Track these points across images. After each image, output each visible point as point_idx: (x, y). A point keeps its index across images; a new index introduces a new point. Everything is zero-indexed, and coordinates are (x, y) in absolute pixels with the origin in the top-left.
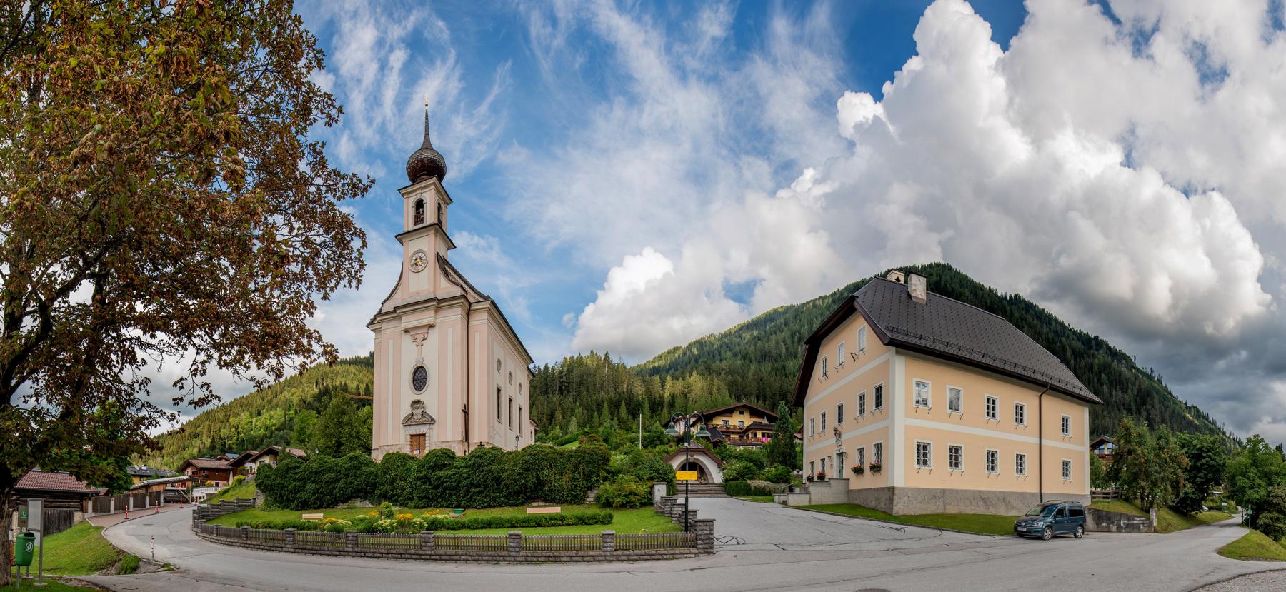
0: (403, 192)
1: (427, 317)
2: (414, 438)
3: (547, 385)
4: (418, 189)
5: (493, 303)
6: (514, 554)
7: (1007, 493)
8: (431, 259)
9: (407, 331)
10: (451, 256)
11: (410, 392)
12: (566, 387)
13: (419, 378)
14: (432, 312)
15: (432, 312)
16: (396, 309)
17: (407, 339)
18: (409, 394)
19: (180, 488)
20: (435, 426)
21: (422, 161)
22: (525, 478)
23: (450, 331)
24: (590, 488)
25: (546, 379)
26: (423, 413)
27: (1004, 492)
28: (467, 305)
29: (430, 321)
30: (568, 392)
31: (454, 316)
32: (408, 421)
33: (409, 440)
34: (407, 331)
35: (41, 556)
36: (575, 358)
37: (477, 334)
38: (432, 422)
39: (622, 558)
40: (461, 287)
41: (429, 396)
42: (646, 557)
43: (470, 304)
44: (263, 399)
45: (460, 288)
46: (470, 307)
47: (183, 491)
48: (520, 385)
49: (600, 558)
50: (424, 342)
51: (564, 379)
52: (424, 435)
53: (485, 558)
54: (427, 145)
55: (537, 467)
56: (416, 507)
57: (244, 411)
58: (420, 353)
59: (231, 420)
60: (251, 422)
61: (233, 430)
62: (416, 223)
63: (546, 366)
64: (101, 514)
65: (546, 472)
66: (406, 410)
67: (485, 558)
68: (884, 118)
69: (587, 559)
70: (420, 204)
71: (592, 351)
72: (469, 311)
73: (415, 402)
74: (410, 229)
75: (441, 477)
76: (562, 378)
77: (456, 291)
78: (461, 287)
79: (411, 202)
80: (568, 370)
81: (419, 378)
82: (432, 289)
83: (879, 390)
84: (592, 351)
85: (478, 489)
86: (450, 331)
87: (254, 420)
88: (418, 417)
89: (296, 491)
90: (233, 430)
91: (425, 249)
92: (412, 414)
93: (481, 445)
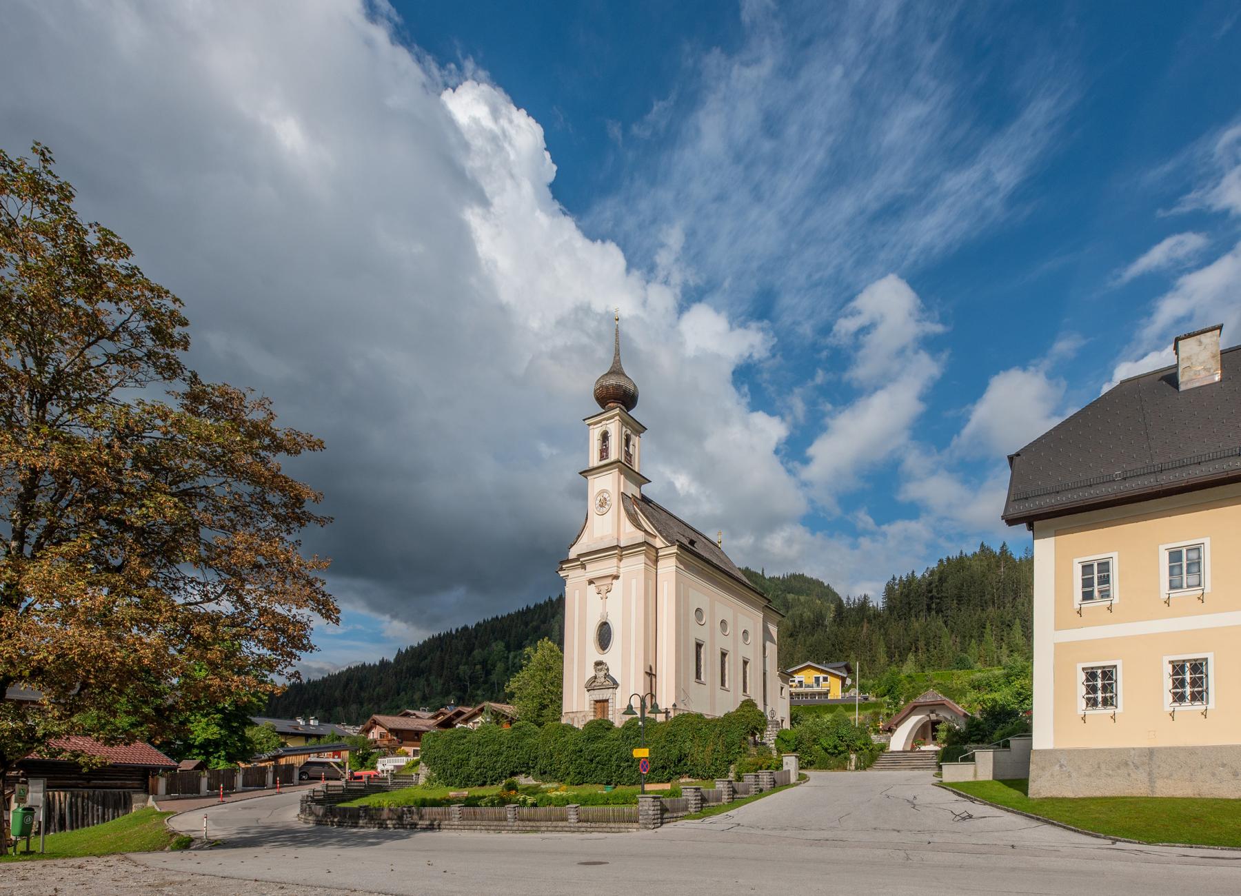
1: (607, 566)
2: (598, 704)
4: (604, 420)
6: (510, 824)
8: (614, 499)
9: (591, 582)
10: (647, 490)
13: (604, 636)
14: (615, 560)
15: (615, 560)
16: (580, 556)
18: (594, 654)
19: (331, 760)
21: (607, 387)
23: (634, 581)
26: (607, 676)
29: (613, 571)
31: (635, 565)
32: (591, 686)
33: (592, 706)
34: (591, 582)
37: (666, 583)
38: (615, 685)
39: (583, 829)
41: (612, 658)
42: (599, 829)
43: (657, 550)
44: (527, 624)
46: (657, 553)
47: (336, 763)
49: (566, 829)
52: (607, 701)
53: (492, 828)
54: (616, 371)
56: (572, 784)
57: (496, 640)
58: (604, 606)
59: (476, 652)
60: (508, 658)
61: (478, 667)
62: (602, 458)
64: (189, 795)
65: (688, 744)
66: (590, 672)
67: (492, 828)
68: (1047, 364)
69: (558, 829)
70: (605, 437)
72: (657, 557)
73: (598, 664)
75: (594, 750)
76: (930, 591)
79: (595, 434)
80: (940, 579)
81: (604, 636)
86: (634, 581)
87: (512, 655)
88: (603, 680)
89: (461, 764)
90: (478, 667)
91: (609, 488)
92: (595, 677)
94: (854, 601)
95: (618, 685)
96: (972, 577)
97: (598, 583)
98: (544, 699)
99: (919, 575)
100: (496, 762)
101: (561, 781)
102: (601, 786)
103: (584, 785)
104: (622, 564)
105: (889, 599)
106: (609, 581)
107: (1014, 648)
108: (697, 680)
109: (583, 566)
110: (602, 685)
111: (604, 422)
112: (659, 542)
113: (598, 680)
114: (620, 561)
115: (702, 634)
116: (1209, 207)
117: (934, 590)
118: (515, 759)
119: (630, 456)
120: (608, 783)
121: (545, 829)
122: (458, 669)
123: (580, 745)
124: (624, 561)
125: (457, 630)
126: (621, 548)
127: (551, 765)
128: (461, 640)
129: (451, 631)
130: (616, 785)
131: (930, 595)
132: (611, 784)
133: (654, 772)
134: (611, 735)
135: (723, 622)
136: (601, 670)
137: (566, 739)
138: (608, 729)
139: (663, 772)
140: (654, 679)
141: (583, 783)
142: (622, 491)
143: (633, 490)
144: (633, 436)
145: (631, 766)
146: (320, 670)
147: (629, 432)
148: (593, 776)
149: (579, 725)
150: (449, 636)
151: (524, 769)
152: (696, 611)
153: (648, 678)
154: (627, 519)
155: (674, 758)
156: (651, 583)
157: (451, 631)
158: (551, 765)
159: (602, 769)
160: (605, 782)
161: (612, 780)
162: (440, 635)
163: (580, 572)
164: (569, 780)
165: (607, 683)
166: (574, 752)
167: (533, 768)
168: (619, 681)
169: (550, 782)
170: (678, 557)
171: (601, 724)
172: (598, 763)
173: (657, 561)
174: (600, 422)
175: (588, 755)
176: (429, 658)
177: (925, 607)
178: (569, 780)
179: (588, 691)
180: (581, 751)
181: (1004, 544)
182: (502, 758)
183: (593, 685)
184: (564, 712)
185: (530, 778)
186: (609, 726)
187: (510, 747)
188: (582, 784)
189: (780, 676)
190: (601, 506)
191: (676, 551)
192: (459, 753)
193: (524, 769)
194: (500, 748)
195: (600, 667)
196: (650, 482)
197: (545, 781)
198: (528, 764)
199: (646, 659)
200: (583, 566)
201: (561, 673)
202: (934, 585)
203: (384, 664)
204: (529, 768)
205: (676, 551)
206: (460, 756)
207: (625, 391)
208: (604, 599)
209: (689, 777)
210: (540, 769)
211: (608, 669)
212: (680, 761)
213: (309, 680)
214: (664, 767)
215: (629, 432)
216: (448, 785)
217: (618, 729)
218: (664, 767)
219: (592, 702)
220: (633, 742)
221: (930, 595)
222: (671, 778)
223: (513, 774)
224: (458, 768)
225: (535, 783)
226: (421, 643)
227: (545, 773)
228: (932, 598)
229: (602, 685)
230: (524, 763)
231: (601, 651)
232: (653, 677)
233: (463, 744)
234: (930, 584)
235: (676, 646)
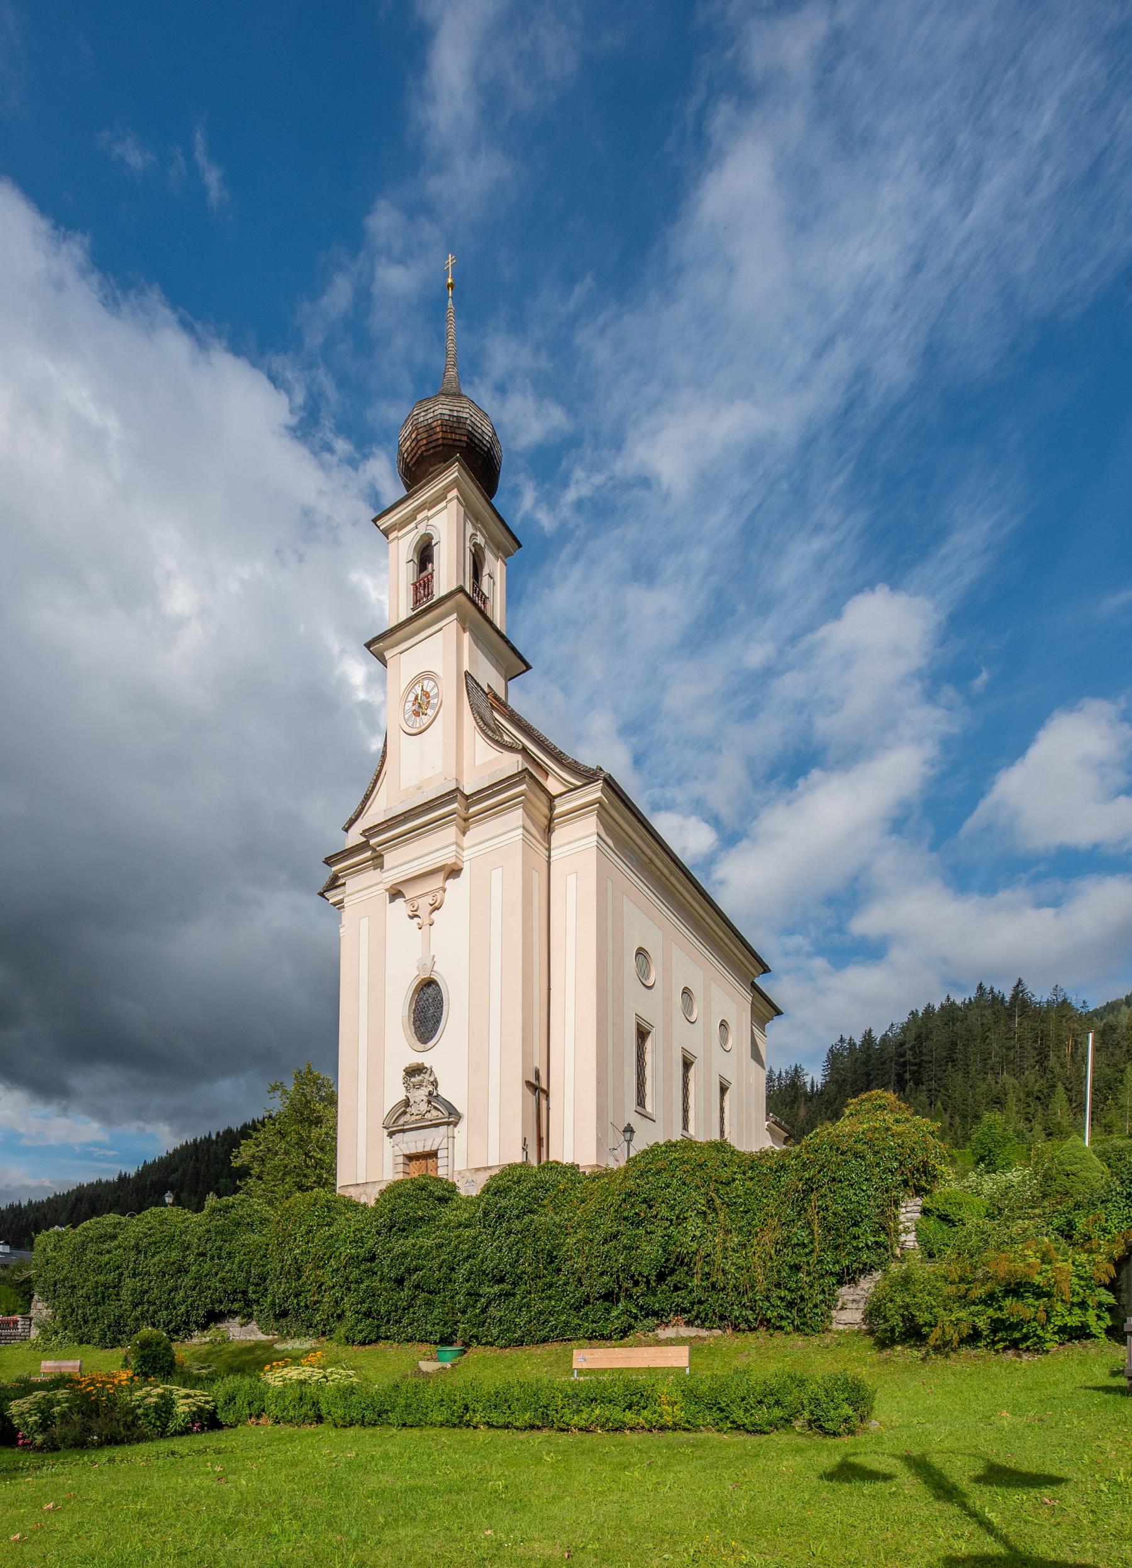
0: (385, 523)
2: (414, 1165)
3: (868, 1074)
5: (610, 784)
12: (913, 1073)
15: (450, 833)
20: (461, 1130)
21: (429, 428)
22: (629, 1248)
23: (497, 875)
24: (847, 1277)
25: (865, 1063)
26: (433, 1098)
29: (446, 857)
30: (918, 1082)
33: (401, 1168)
34: (396, 894)
36: (937, 1007)
38: (453, 1117)
40: (524, 751)
43: (551, 798)
45: (518, 757)
46: (552, 809)
48: (723, 1024)
51: (909, 1056)
55: (664, 1211)
56: (349, 1340)
58: (427, 943)
63: (869, 1034)
65: (694, 1225)
66: (395, 1092)
70: (425, 555)
71: (980, 987)
72: (551, 820)
73: (414, 1071)
75: (405, 1255)
76: (903, 1055)
77: (512, 763)
78: (524, 751)
79: (404, 546)
80: (919, 1037)
82: (452, 772)
84: (980, 987)
85: (497, 1288)
86: (497, 875)
89: (104, 1294)
91: (438, 669)
92: (407, 1103)
94: (780, 1075)
95: (459, 1117)
96: (970, 1031)
97: (409, 893)
98: (305, 1176)
99: (877, 1035)
100: (176, 1289)
101: (324, 1334)
102: (426, 1348)
103: (381, 1344)
104: (467, 841)
105: (832, 1069)
106: (437, 881)
107: (1055, 1130)
108: (640, 1109)
109: (377, 861)
110: (423, 1119)
111: (420, 517)
114: (464, 833)
115: (650, 1008)
117: (909, 1053)
118: (215, 1282)
120: (446, 1341)
122: (217, 1183)
123: (371, 1242)
124: (476, 832)
125: (218, 1134)
126: (467, 797)
127: (297, 1296)
128: (223, 1145)
129: (210, 1135)
130: (467, 1345)
131: (902, 1060)
132: (451, 1344)
133: (578, 1309)
134: (448, 1214)
135: (686, 992)
136: (420, 1085)
137: (333, 1229)
138: (442, 1200)
139: (608, 1311)
140: (544, 1103)
141: (379, 1338)
142: (466, 667)
143: (489, 676)
144: (489, 556)
145: (509, 1295)
146: (42, 1188)
147: (480, 540)
148: (405, 1321)
149: (369, 1197)
150: (208, 1140)
151: (236, 1306)
152: (638, 954)
153: (532, 1099)
155: (646, 1268)
157: (210, 1135)
158: (297, 1296)
159: (428, 1303)
160: (437, 1337)
161: (454, 1333)
162: (195, 1140)
163: (371, 876)
164: (341, 1331)
165: (434, 1113)
166: (355, 1261)
167: (257, 1302)
168: (461, 1107)
169: (297, 1335)
171: (423, 1188)
172: (417, 1287)
173: (549, 830)
174: (411, 518)
175: (391, 1267)
176: (180, 1170)
177: (894, 1077)
178: (341, 1331)
179: (391, 1134)
180: (373, 1258)
181: (1020, 982)
182: (187, 1281)
183: (401, 1122)
184: (338, 1186)
185: (253, 1325)
186: (446, 1194)
187: (203, 1255)
188: (375, 1341)
189: (769, 1129)
190: (417, 714)
191: (599, 794)
192: (99, 1270)
193: (236, 1306)
194: (185, 1257)
195: (416, 1079)
197: (286, 1336)
198: (245, 1293)
199: (526, 1055)
200: (377, 861)
201: (334, 1128)
202: (908, 1045)
203: (123, 1179)
204: (248, 1303)
205: (599, 794)
206: (101, 1278)
207: (470, 435)
209: (689, 1323)
210: (273, 1304)
211: (435, 1084)
212: (661, 1277)
213: (30, 1202)
214: (610, 1297)
215: (480, 540)
216: (81, 1342)
217: (469, 1201)
218: (610, 1297)
219: (401, 1159)
220: (517, 1225)
221: (902, 1060)
222: (631, 1327)
223: (214, 1317)
224: (98, 1304)
225: (264, 1337)
226: (171, 1151)
227: (284, 1314)
228: (904, 1064)
229: (423, 1119)
230: (235, 1292)
231: (421, 1047)
233: (109, 1252)
234: (902, 1044)
235: (598, 1022)
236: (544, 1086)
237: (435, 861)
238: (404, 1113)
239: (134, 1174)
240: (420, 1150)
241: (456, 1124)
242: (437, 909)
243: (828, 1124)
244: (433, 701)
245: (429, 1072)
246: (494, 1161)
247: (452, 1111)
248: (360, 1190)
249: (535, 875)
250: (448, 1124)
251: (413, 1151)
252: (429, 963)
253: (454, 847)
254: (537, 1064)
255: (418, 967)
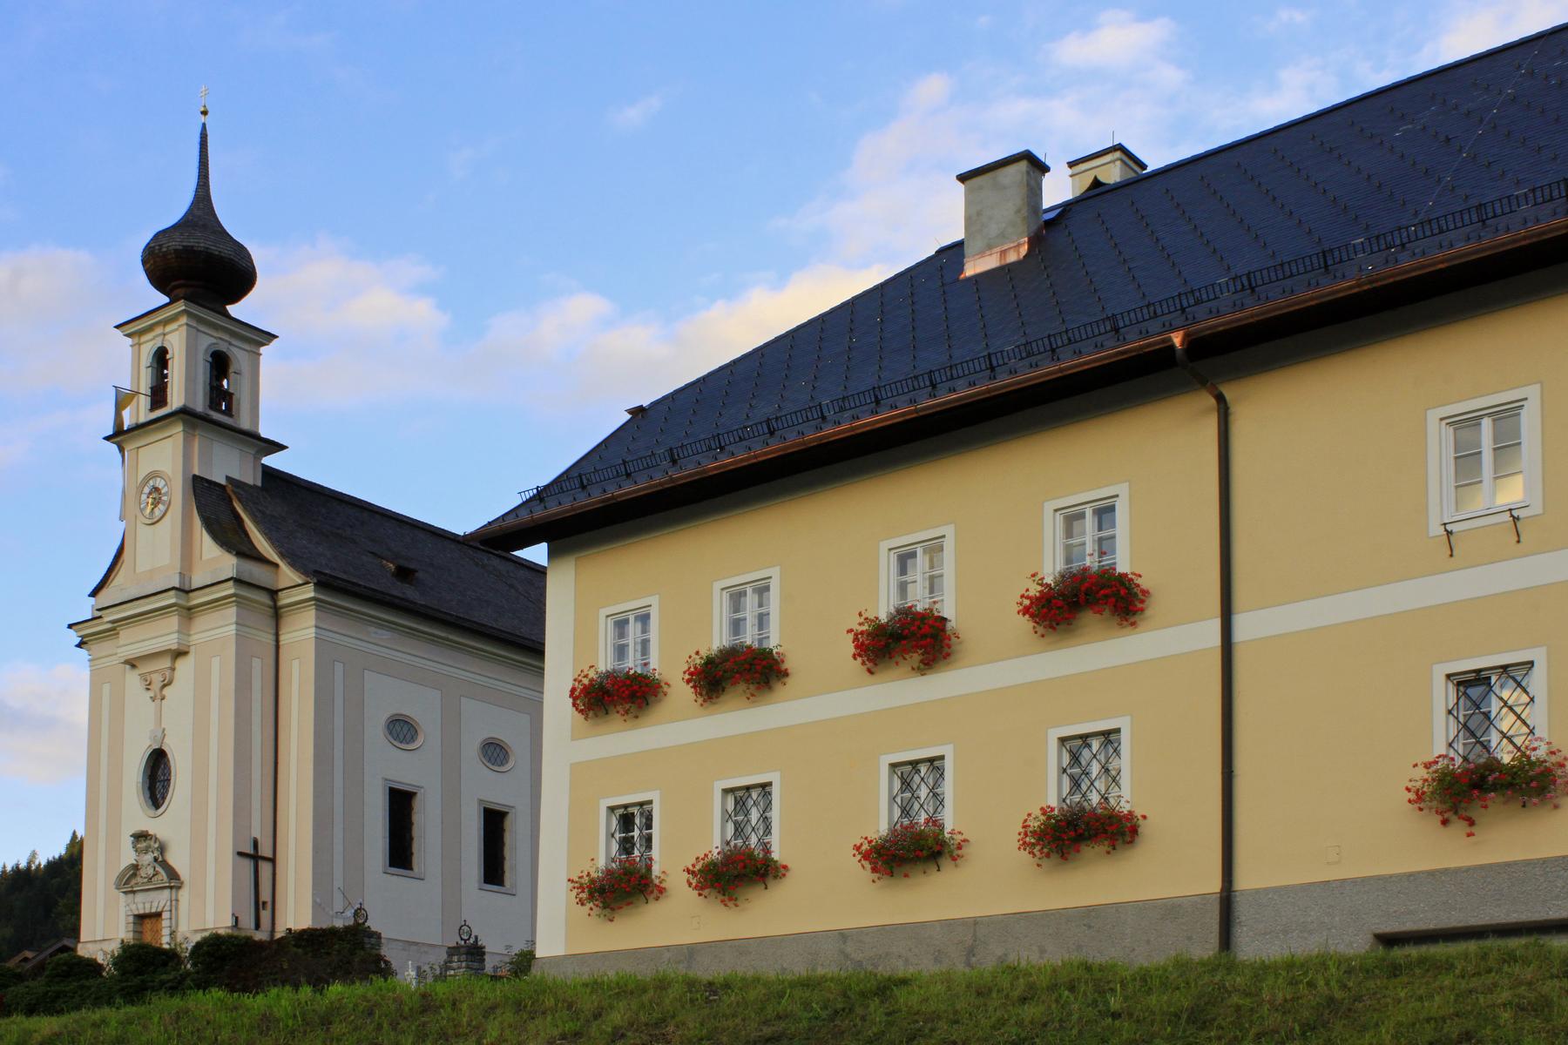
7: (990, 921)
9: (132, 664)
11: (382, 736)
17: (133, 679)
23: (216, 662)
27: (976, 922)
28: (264, 598)
29: (171, 641)
32: (129, 880)
34: (132, 664)
35: (1098, 195)
37: (296, 664)
41: (169, 825)
43: (273, 593)
46: (275, 601)
50: (166, 691)
52: (158, 915)
66: (128, 856)
73: (140, 837)
74: (142, 420)
83: (494, 822)
86: (216, 662)
93: (369, 927)
97: (145, 668)
106: (165, 663)
111: (159, 330)
112: (288, 575)
113: (143, 873)
116: (765, 649)
119: (227, 396)
121: (174, 898)
136: (146, 851)
153: (248, 865)
154: (204, 532)
156: (259, 669)
170: (318, 603)
174: (150, 328)
183: (133, 882)
191: (312, 594)
195: (142, 845)
196: (275, 337)
208: (158, 701)
211: (162, 849)
219: (131, 919)
231: (152, 812)
232: (265, 868)
236: (267, 852)
237: (164, 644)
238: (134, 875)
239: (43, 863)
240: (147, 911)
241: (179, 888)
242: (170, 683)
243: (24, 1018)
244: (164, 498)
245: (153, 839)
246: (210, 925)
247: (173, 874)
248: (98, 946)
249: (256, 663)
250: (171, 888)
251: (141, 912)
252: (159, 734)
253: (176, 635)
254: (256, 833)
255: (150, 738)
